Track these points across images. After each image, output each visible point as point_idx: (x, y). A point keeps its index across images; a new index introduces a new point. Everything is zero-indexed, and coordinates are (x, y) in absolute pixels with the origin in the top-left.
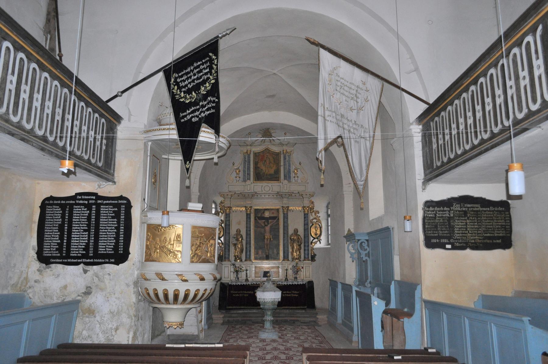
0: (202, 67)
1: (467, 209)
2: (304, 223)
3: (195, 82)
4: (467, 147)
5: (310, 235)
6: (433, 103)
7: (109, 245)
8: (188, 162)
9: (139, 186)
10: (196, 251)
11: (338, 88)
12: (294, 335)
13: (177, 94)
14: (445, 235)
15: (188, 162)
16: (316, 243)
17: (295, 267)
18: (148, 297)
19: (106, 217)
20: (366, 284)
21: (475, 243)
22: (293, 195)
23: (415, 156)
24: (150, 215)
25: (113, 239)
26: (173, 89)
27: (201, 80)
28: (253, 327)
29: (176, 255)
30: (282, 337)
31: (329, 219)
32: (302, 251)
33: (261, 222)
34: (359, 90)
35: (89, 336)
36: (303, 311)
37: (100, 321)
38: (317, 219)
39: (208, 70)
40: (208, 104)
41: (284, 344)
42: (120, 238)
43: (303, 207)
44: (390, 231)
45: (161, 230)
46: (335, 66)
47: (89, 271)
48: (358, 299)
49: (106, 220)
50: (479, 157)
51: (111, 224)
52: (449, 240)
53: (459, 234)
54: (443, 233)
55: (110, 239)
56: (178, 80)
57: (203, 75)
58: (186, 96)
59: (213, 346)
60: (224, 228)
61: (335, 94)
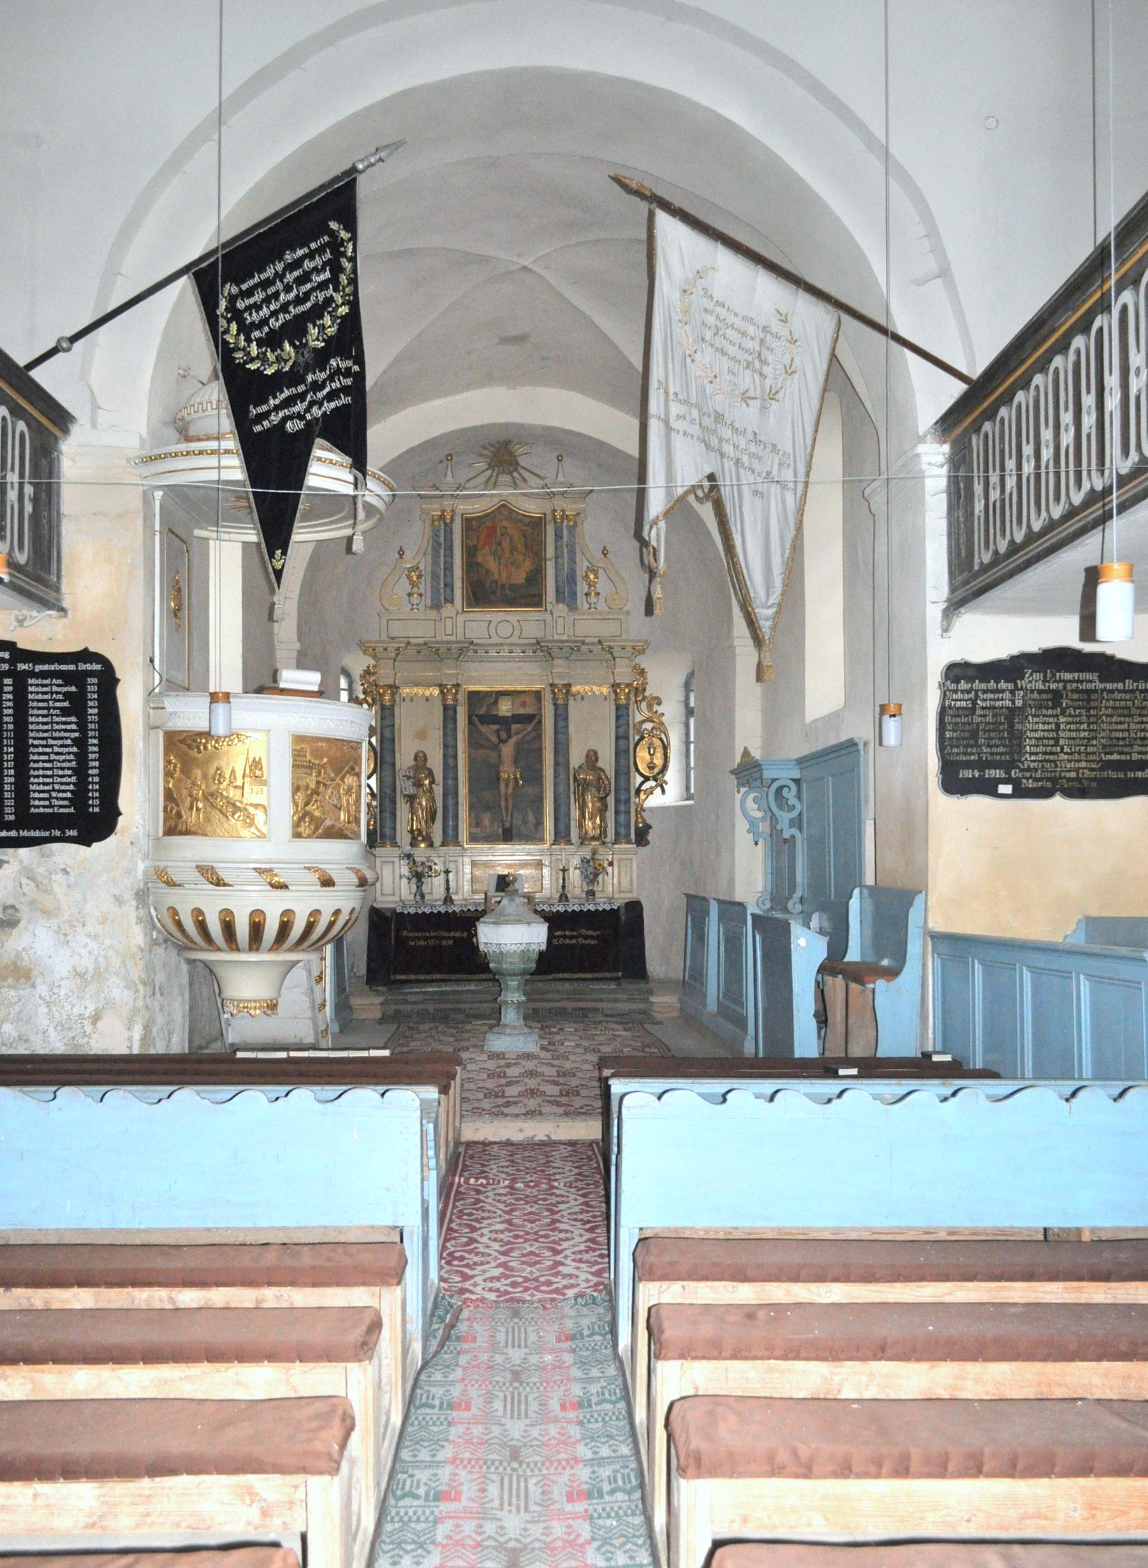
0: (308, 265)
1: (1061, 685)
2: (617, 733)
3: (290, 313)
4: (1057, 512)
5: (632, 769)
6: (978, 379)
7: (59, 791)
8: (279, 552)
9: (137, 622)
10: (307, 804)
11: (708, 335)
12: (585, 1043)
13: (237, 349)
14: (998, 758)
15: (279, 552)
16: (650, 792)
17: (588, 861)
18: (178, 934)
19: (45, 712)
20: (790, 905)
21: (1078, 779)
22: (584, 648)
23: (928, 533)
24: (172, 704)
25: (70, 772)
26: (227, 331)
27: (309, 305)
28: (469, 1027)
29: (250, 821)
30: (550, 1047)
31: (692, 721)
32: (610, 815)
33: (489, 730)
34: (769, 338)
35: (20, 1038)
36: (613, 986)
37: (48, 998)
38: (653, 722)
39: (328, 274)
40: (331, 378)
41: (556, 1062)
42: (90, 772)
43: (613, 686)
44: (858, 750)
45: (205, 748)
46: (699, 267)
47: (7, 862)
48: (758, 937)
49: (45, 720)
50: (1081, 539)
51: (60, 731)
52: (1008, 772)
53: (1036, 754)
54: (992, 754)
55: (61, 773)
56: (240, 305)
57: (313, 289)
58: (265, 354)
59: (364, 1054)
60: (378, 750)
61: (699, 353)
